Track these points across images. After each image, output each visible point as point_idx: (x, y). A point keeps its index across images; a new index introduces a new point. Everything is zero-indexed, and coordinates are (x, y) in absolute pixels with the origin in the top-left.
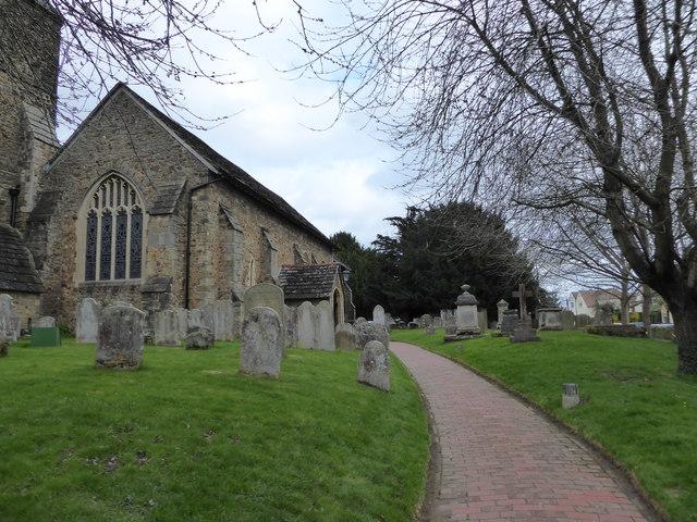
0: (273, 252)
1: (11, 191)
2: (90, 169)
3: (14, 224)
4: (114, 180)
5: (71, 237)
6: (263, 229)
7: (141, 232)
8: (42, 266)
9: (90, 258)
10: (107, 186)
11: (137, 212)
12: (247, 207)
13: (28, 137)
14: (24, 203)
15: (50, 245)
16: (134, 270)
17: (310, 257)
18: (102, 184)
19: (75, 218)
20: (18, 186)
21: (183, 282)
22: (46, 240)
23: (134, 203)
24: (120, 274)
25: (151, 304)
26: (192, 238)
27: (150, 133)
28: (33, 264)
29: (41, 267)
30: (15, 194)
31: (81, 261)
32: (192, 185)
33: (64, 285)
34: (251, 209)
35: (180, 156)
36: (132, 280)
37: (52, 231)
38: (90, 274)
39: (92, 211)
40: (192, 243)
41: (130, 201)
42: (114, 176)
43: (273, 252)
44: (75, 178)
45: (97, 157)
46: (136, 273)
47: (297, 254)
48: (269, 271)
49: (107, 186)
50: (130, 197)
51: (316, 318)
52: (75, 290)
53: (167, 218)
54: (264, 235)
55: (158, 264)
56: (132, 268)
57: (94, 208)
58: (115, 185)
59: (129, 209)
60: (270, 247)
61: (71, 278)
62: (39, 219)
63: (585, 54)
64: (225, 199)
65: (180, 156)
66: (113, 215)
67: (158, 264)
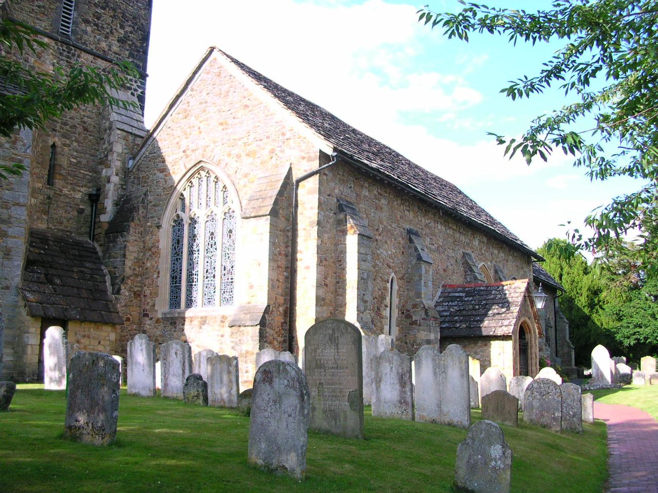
0: (424, 267)
1: (90, 196)
3: (93, 237)
5: (151, 250)
6: (410, 232)
8: (119, 289)
11: (228, 214)
12: (383, 202)
13: (110, 128)
14: (103, 211)
15: (129, 263)
17: (492, 273)
18: (189, 180)
19: (159, 227)
20: (99, 190)
21: (285, 312)
22: (124, 256)
23: (225, 203)
27: (246, 106)
28: (110, 289)
29: (118, 292)
30: (95, 199)
33: (147, 315)
37: (132, 243)
39: (178, 216)
41: (203, 202)
43: (424, 267)
46: (227, 299)
47: (468, 268)
48: (419, 295)
50: (220, 194)
51: (366, 410)
52: (158, 321)
54: (411, 241)
57: (180, 212)
58: (205, 179)
60: (419, 258)
61: (154, 305)
62: (119, 226)
63: (24, 30)
64: (347, 191)
65: (283, 134)
66: (184, 222)
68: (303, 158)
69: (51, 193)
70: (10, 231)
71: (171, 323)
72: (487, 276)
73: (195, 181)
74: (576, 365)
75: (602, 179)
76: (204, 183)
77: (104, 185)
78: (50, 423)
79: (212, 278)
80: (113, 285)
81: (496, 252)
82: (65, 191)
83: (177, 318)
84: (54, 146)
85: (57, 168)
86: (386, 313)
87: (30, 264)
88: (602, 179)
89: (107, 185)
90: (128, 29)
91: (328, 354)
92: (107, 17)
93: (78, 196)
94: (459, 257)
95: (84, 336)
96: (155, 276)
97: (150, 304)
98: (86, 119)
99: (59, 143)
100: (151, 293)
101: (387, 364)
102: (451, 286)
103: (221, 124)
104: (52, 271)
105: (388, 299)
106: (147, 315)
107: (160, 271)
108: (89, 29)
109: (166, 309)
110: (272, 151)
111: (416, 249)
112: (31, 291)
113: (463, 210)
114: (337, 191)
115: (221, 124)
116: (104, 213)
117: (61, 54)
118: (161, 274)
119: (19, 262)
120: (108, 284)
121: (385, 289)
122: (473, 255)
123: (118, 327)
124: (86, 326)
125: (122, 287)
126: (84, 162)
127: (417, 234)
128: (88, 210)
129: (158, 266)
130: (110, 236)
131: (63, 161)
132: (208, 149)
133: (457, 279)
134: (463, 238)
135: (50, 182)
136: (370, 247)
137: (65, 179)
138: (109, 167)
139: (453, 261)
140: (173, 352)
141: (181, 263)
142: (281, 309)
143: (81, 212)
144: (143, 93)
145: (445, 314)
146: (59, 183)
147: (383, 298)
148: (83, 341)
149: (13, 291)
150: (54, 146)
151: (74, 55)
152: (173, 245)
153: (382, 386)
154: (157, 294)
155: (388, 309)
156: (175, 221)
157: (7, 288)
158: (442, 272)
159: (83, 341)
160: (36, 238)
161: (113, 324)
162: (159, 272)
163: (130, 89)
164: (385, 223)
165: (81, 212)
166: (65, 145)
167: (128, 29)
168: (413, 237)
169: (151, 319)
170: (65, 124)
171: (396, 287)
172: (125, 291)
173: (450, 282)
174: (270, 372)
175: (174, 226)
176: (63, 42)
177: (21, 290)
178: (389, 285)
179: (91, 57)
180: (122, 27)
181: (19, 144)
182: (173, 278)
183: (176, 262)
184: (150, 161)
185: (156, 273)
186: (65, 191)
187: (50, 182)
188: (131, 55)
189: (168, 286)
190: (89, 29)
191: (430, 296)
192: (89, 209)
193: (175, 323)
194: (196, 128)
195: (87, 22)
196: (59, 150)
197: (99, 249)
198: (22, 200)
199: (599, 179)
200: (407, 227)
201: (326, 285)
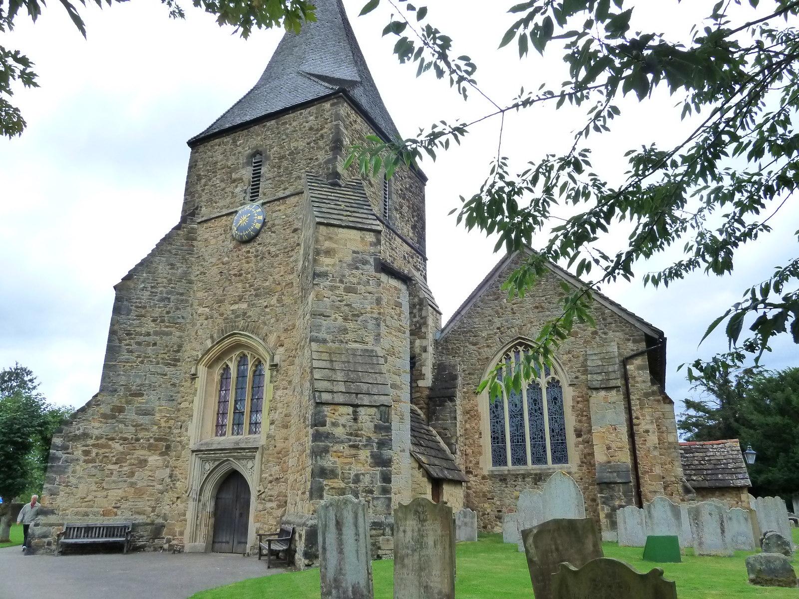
2: (489, 337)
4: (521, 349)
7: (561, 407)
9: (497, 439)
10: (512, 354)
14: (421, 376)
16: (558, 454)
18: (506, 354)
23: (547, 374)
24: (520, 460)
25: (612, 498)
26: (634, 415)
31: (486, 442)
32: (627, 353)
33: (471, 472)
34: (386, 261)
35: (604, 319)
36: (535, 466)
38: (499, 458)
40: (635, 421)
42: (521, 344)
44: (474, 348)
45: (497, 322)
49: (512, 354)
52: (484, 478)
53: (614, 392)
55: (609, 448)
56: (554, 452)
59: (543, 382)
61: (478, 463)
67: (609, 448)
68: (629, 340)
71: (501, 480)
75: (737, 248)
77: (420, 355)
79: (540, 439)
83: (506, 475)
88: (737, 248)
89: (424, 355)
96: (477, 436)
97: (474, 462)
100: (473, 452)
103: (537, 307)
107: (482, 432)
110: (595, 333)
115: (537, 307)
116: (424, 379)
129: (478, 427)
130: (436, 401)
132: (524, 328)
144: (426, 274)
152: (490, 409)
154: (480, 453)
162: (480, 434)
169: (476, 476)
175: (528, 389)
182: (494, 438)
183: (496, 424)
184: (459, 334)
185: (478, 433)
193: (505, 480)
194: (509, 309)
199: (633, 93)
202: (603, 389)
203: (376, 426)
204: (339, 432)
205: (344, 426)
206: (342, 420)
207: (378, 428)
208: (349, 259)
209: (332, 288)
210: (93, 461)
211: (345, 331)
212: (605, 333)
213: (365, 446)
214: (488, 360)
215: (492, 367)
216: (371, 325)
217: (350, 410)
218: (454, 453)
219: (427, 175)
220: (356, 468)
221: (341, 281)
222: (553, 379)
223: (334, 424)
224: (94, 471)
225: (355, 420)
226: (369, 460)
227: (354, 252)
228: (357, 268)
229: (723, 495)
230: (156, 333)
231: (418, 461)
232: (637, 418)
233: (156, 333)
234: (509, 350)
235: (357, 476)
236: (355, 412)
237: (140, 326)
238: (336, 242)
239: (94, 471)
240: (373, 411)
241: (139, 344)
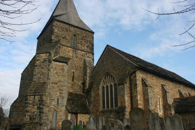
1: (82, 83)
5: (98, 95)
6: (162, 85)
8: (90, 105)
10: (107, 77)
12: (154, 78)
14: (86, 86)
18: (105, 77)
23: (114, 82)
30: (84, 84)
33: (97, 111)
42: (108, 74)
44: (99, 77)
47: (180, 94)
54: (163, 87)
55: (121, 102)
57: (104, 85)
61: (99, 108)
64: (144, 76)
65: (126, 63)
67: (121, 102)
69: (73, 83)
70: (63, 92)
72: (187, 95)
73: (107, 77)
74: (115, 107)
76: (109, 77)
78: (182, 126)
80: (89, 104)
81: (188, 88)
82: (77, 82)
84: (73, 72)
85: (74, 77)
86: (158, 107)
87: (68, 100)
90: (89, 44)
91: (136, 118)
92: (83, 41)
93: (80, 83)
94: (178, 91)
95: (82, 117)
98: (80, 65)
99: (74, 71)
101: (157, 121)
102: (176, 98)
104: (74, 101)
105: (158, 103)
106: (97, 111)
108: (79, 45)
109: (102, 109)
110: (124, 68)
111: (165, 89)
112: (69, 106)
113: (177, 78)
114: (141, 76)
117: (73, 51)
118: (100, 101)
119: (66, 100)
120: (88, 104)
121: (157, 100)
122: (181, 90)
123: (90, 114)
124: (82, 115)
125: (91, 104)
126: (81, 75)
127: (164, 85)
128: (82, 87)
131: (76, 75)
133: (178, 96)
134: (178, 85)
135: (73, 80)
136: (151, 89)
137: (76, 79)
138: (87, 76)
139: (176, 92)
140: (100, 119)
141: (105, 97)
142: (130, 107)
143: (80, 87)
144: (93, 58)
145: (175, 106)
146: (75, 81)
147: (157, 103)
148: (82, 118)
149: (65, 107)
150: (73, 72)
151: (76, 51)
153: (156, 127)
155: (159, 106)
156: (103, 87)
157: (63, 106)
158: (173, 95)
159: (82, 118)
160: (70, 94)
161: (89, 114)
163: (90, 57)
164: (155, 83)
165: (80, 87)
166: (76, 72)
167: (89, 44)
168: (163, 86)
170: (76, 67)
171: (160, 100)
172: (92, 105)
173: (176, 97)
174: (113, 124)
176: (74, 48)
177: (66, 107)
178: (158, 99)
179: (80, 51)
180: (87, 44)
181: (64, 72)
186: (77, 82)
187: (73, 80)
188: (90, 50)
189: (102, 103)
190: (79, 45)
191: (170, 101)
192: (82, 86)
195: (79, 43)
196: (74, 73)
197: (85, 95)
198: (66, 85)
200: (162, 84)
201: (141, 100)
202: (121, 84)
203: (39, 100)
204: (30, 102)
205: (32, 101)
206: (31, 99)
207: (39, 101)
208: (42, 61)
209: (38, 69)
210: (17, 111)
211: (40, 78)
212: (126, 68)
213: (36, 105)
214: (102, 79)
215: (102, 82)
216: (46, 76)
217: (33, 96)
218: (90, 105)
219: (94, 32)
220: (34, 110)
221: (40, 67)
222: (115, 83)
223: (30, 100)
224: (17, 114)
225: (34, 99)
226: (37, 108)
227: (44, 59)
228: (44, 63)
229: (189, 114)
230: (28, 83)
231: (67, 108)
232: (133, 92)
233: (28, 83)
234: (106, 76)
235: (34, 112)
236: (34, 97)
237: (26, 82)
238: (40, 57)
239: (17, 114)
240: (38, 96)
241: (25, 86)
